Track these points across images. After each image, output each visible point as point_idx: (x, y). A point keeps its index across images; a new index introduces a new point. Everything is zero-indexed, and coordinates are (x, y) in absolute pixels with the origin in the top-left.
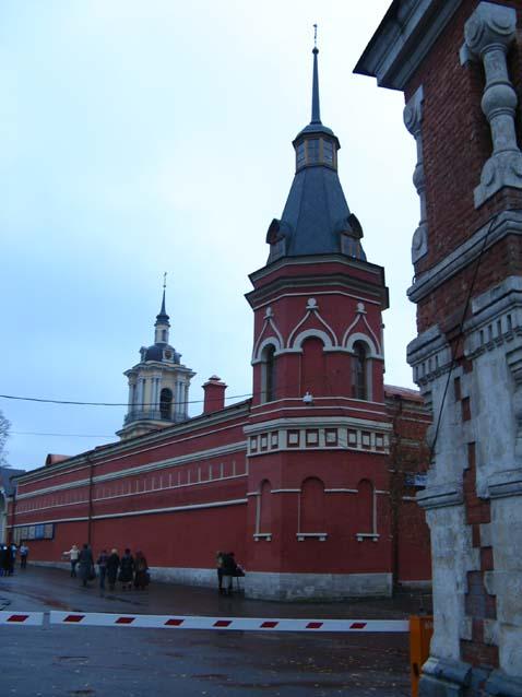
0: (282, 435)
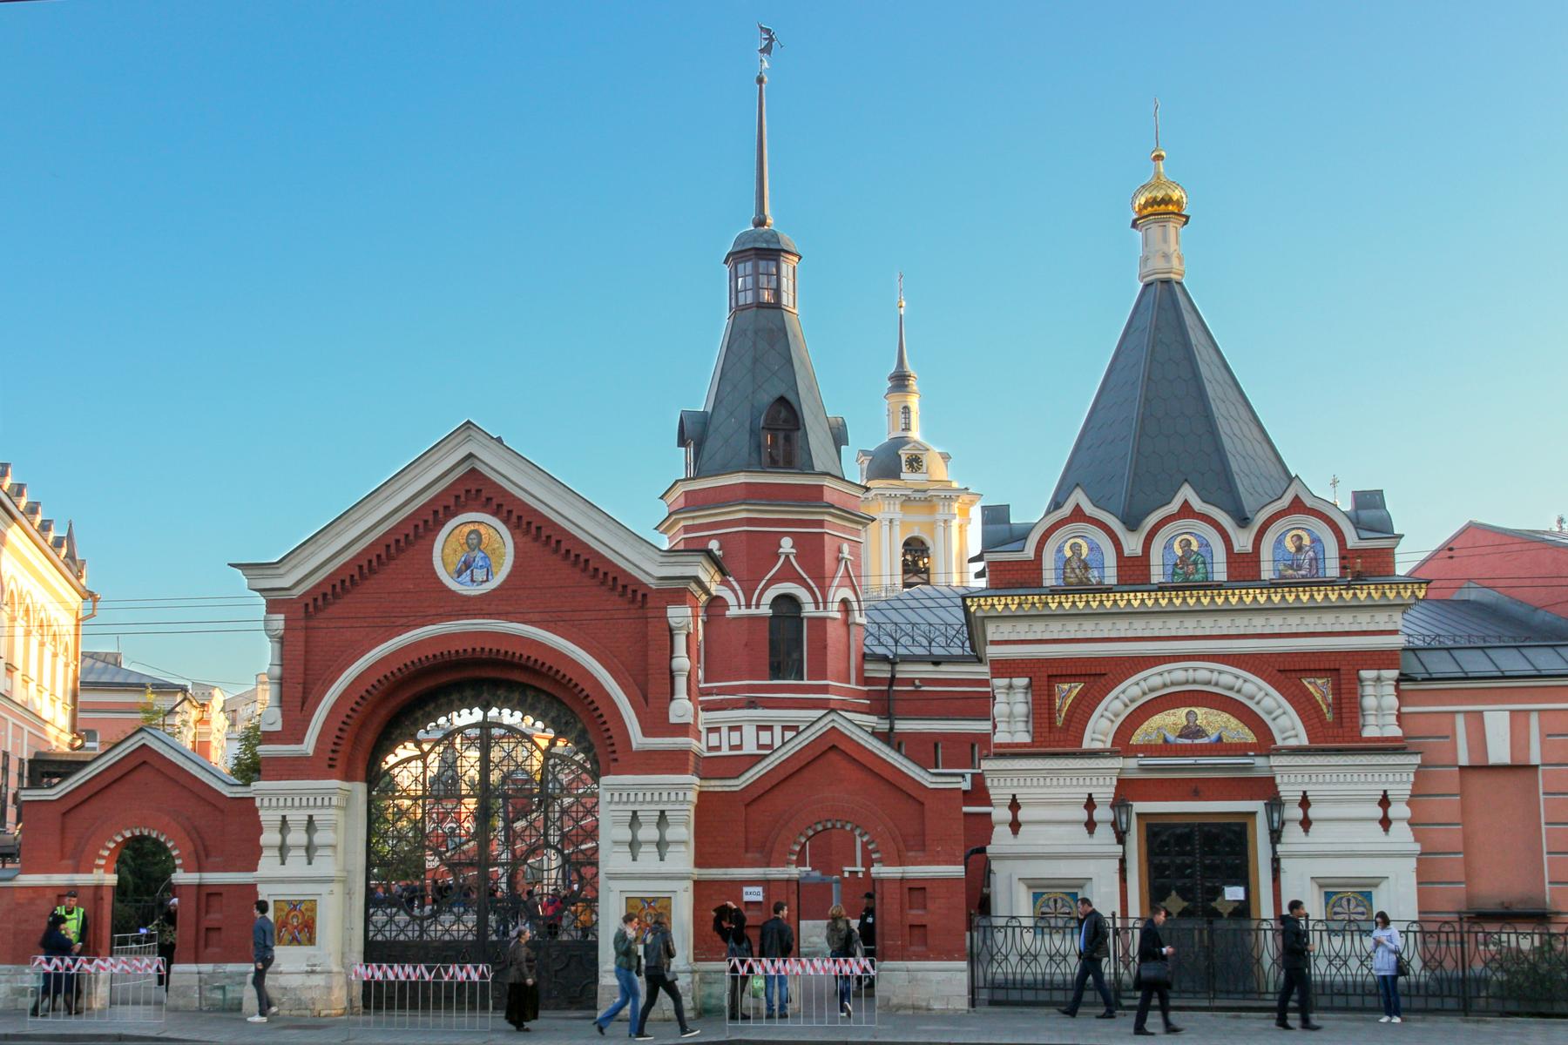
0: (749, 731)
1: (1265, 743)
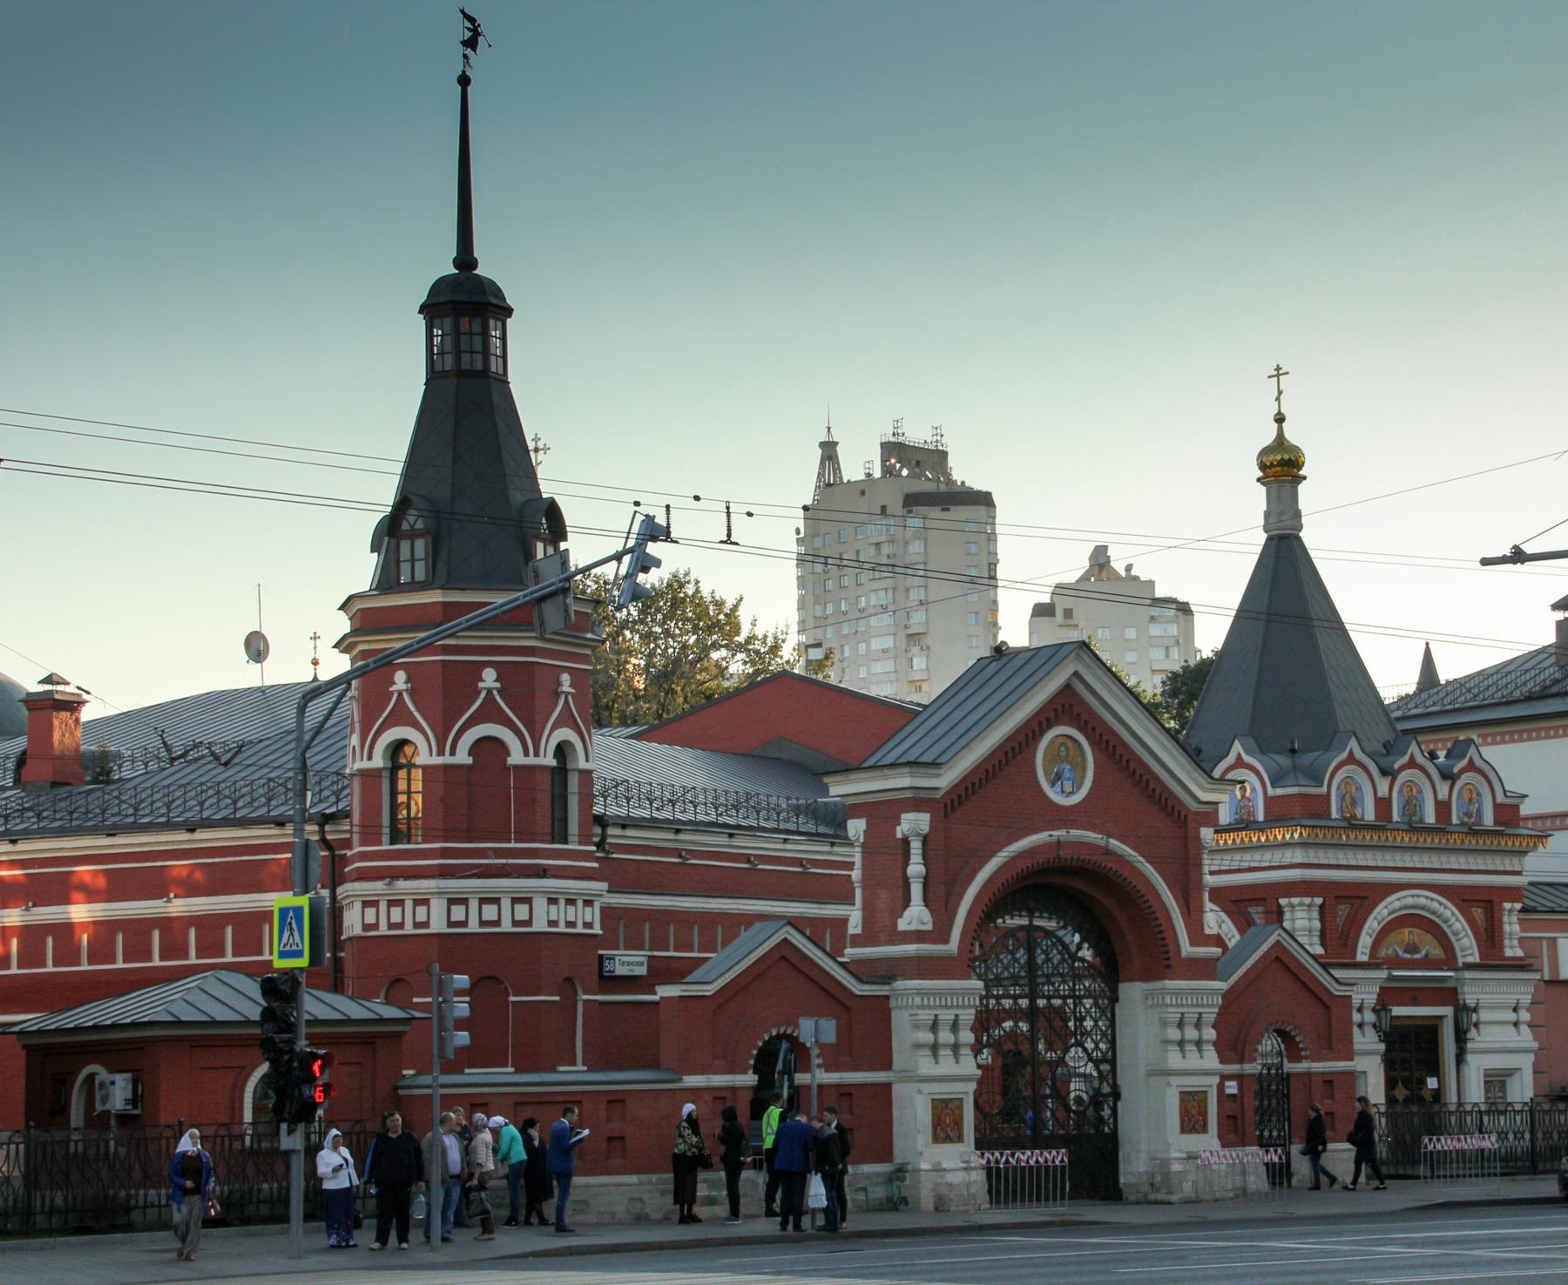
0: (438, 907)
1: (1450, 961)
